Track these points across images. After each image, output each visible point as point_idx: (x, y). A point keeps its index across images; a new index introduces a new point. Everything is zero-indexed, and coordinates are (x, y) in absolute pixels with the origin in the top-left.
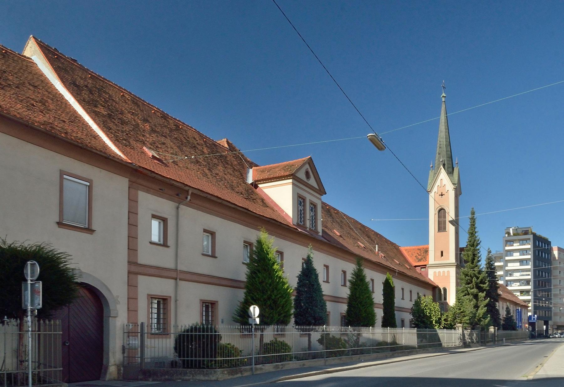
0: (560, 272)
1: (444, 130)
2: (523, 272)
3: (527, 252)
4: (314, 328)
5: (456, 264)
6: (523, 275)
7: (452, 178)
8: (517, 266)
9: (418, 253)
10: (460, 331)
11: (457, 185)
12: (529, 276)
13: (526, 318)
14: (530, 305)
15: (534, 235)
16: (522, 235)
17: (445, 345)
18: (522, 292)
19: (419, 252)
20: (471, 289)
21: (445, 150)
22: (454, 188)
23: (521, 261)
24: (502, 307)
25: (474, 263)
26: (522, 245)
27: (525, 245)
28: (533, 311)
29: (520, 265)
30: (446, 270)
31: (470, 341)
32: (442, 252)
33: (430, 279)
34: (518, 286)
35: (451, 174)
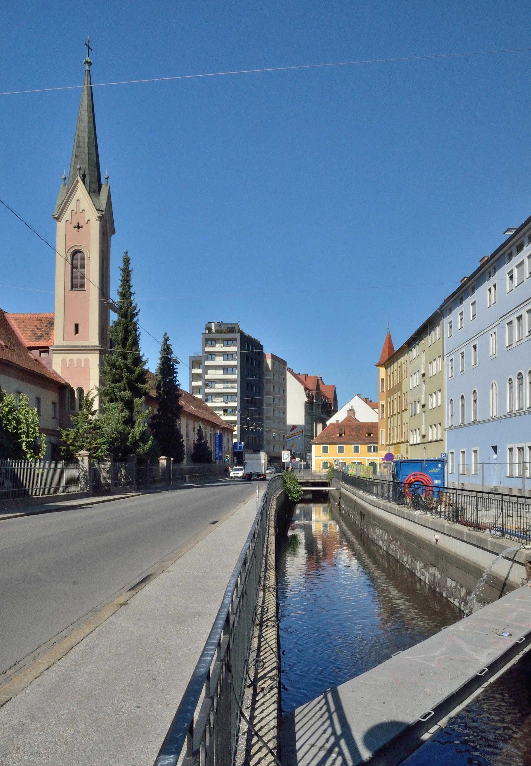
0: (274, 387)
1: (86, 118)
2: (228, 383)
3: (232, 357)
5: (100, 348)
6: (228, 388)
7: (97, 200)
8: (219, 374)
9: (36, 326)
10: (84, 464)
11: (104, 213)
12: (235, 389)
13: (231, 447)
14: (236, 428)
15: (242, 334)
16: (227, 333)
17: (37, 494)
18: (225, 410)
19: (38, 323)
20: (120, 391)
21: (87, 152)
22: (99, 217)
23: (225, 369)
24: (185, 427)
25: (126, 345)
26: (227, 346)
27: (230, 346)
29: (224, 374)
30: (83, 356)
31: (110, 482)
32: (77, 326)
33: (55, 372)
34: (221, 402)
35: (95, 194)
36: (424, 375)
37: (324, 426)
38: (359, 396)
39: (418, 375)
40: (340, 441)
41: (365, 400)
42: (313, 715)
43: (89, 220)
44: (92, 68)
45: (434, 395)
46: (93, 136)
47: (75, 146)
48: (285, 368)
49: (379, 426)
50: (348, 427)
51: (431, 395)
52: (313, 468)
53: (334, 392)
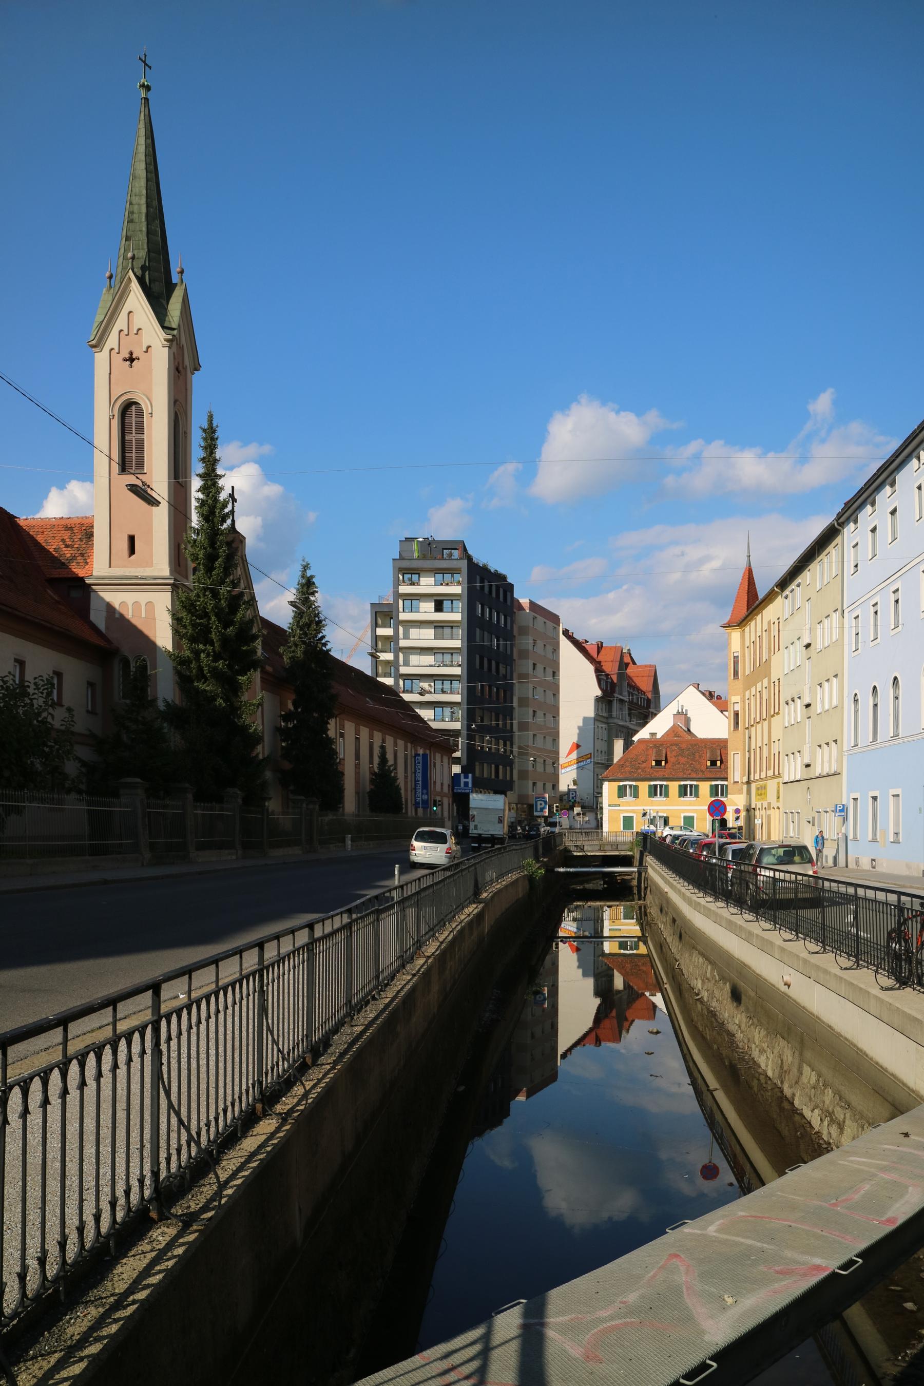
0: (534, 665)
4: (6, 794)
5: (172, 581)
9: (63, 541)
13: (447, 782)
19: (66, 535)
21: (144, 229)
23: (438, 626)
28: (464, 762)
30: (144, 596)
32: (132, 539)
36: (808, 646)
37: (628, 744)
38: (697, 686)
39: (799, 646)
40: (656, 774)
41: (710, 696)
42: (206, 1079)
43: (149, 347)
44: (150, 95)
45: (826, 685)
46: (155, 203)
47: (126, 222)
48: (556, 629)
49: (730, 745)
50: (674, 748)
51: (820, 685)
52: (606, 828)
53: (653, 678)
